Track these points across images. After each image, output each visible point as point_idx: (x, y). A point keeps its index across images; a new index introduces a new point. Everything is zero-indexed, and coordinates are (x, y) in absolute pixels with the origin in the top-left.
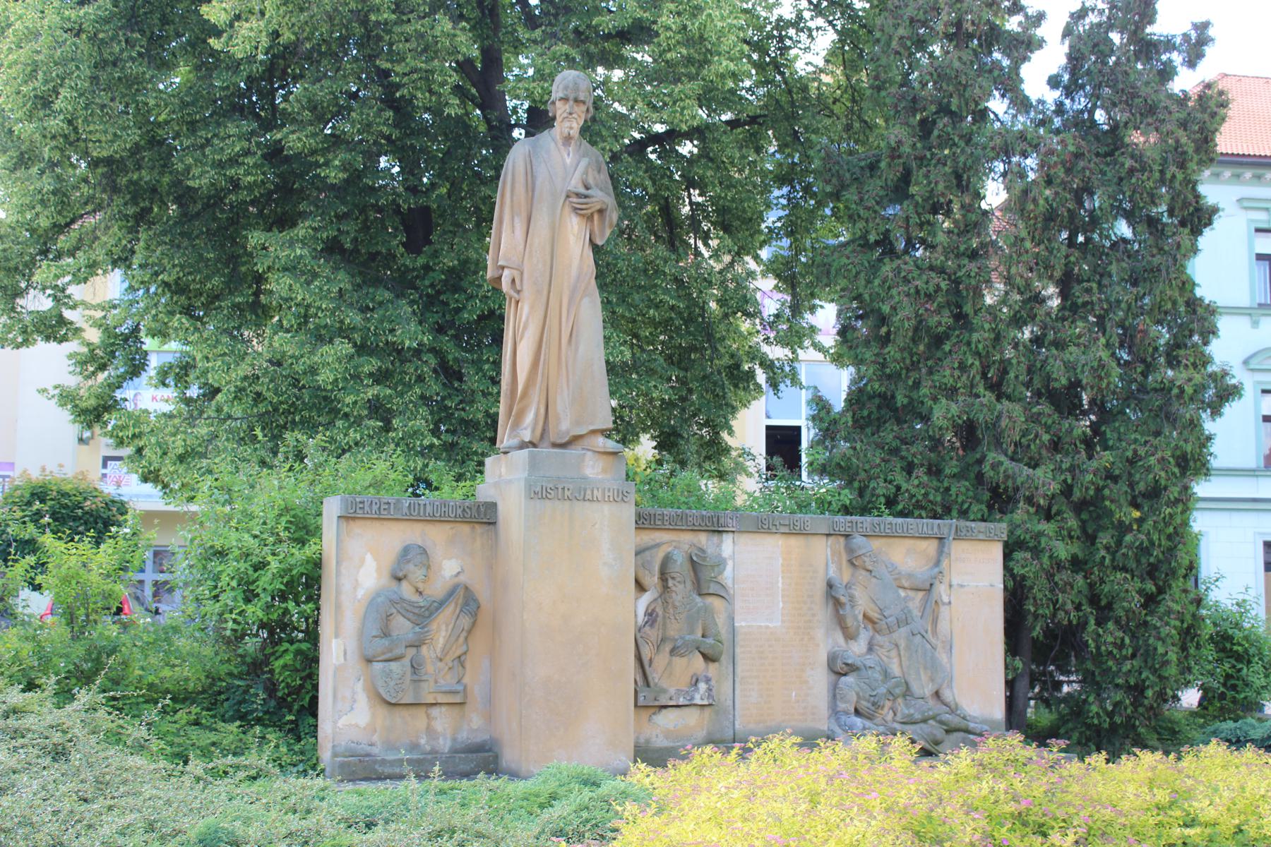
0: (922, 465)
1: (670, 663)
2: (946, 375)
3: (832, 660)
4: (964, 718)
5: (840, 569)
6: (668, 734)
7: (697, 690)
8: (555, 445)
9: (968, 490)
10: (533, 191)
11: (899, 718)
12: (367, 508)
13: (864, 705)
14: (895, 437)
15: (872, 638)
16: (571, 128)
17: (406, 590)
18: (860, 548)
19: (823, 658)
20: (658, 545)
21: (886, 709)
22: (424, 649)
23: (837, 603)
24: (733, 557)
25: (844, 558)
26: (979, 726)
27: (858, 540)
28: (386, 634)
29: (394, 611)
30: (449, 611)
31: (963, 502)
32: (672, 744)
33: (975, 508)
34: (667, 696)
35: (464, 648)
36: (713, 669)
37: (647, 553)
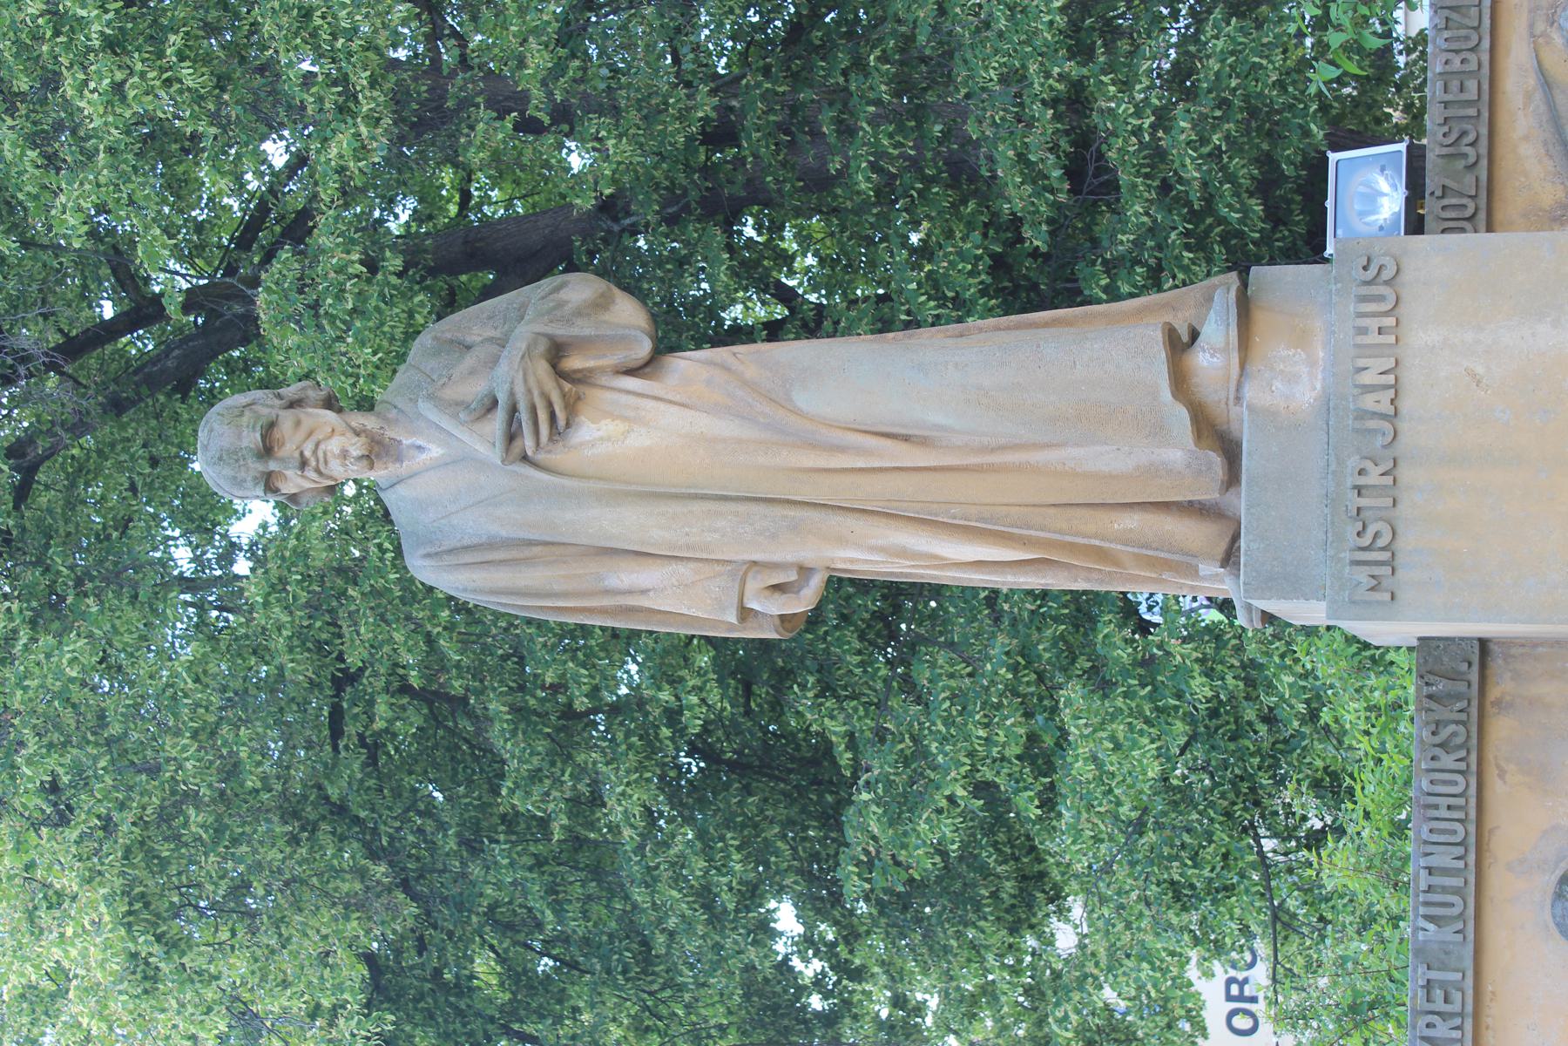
10: (530, 543)
16: (344, 454)
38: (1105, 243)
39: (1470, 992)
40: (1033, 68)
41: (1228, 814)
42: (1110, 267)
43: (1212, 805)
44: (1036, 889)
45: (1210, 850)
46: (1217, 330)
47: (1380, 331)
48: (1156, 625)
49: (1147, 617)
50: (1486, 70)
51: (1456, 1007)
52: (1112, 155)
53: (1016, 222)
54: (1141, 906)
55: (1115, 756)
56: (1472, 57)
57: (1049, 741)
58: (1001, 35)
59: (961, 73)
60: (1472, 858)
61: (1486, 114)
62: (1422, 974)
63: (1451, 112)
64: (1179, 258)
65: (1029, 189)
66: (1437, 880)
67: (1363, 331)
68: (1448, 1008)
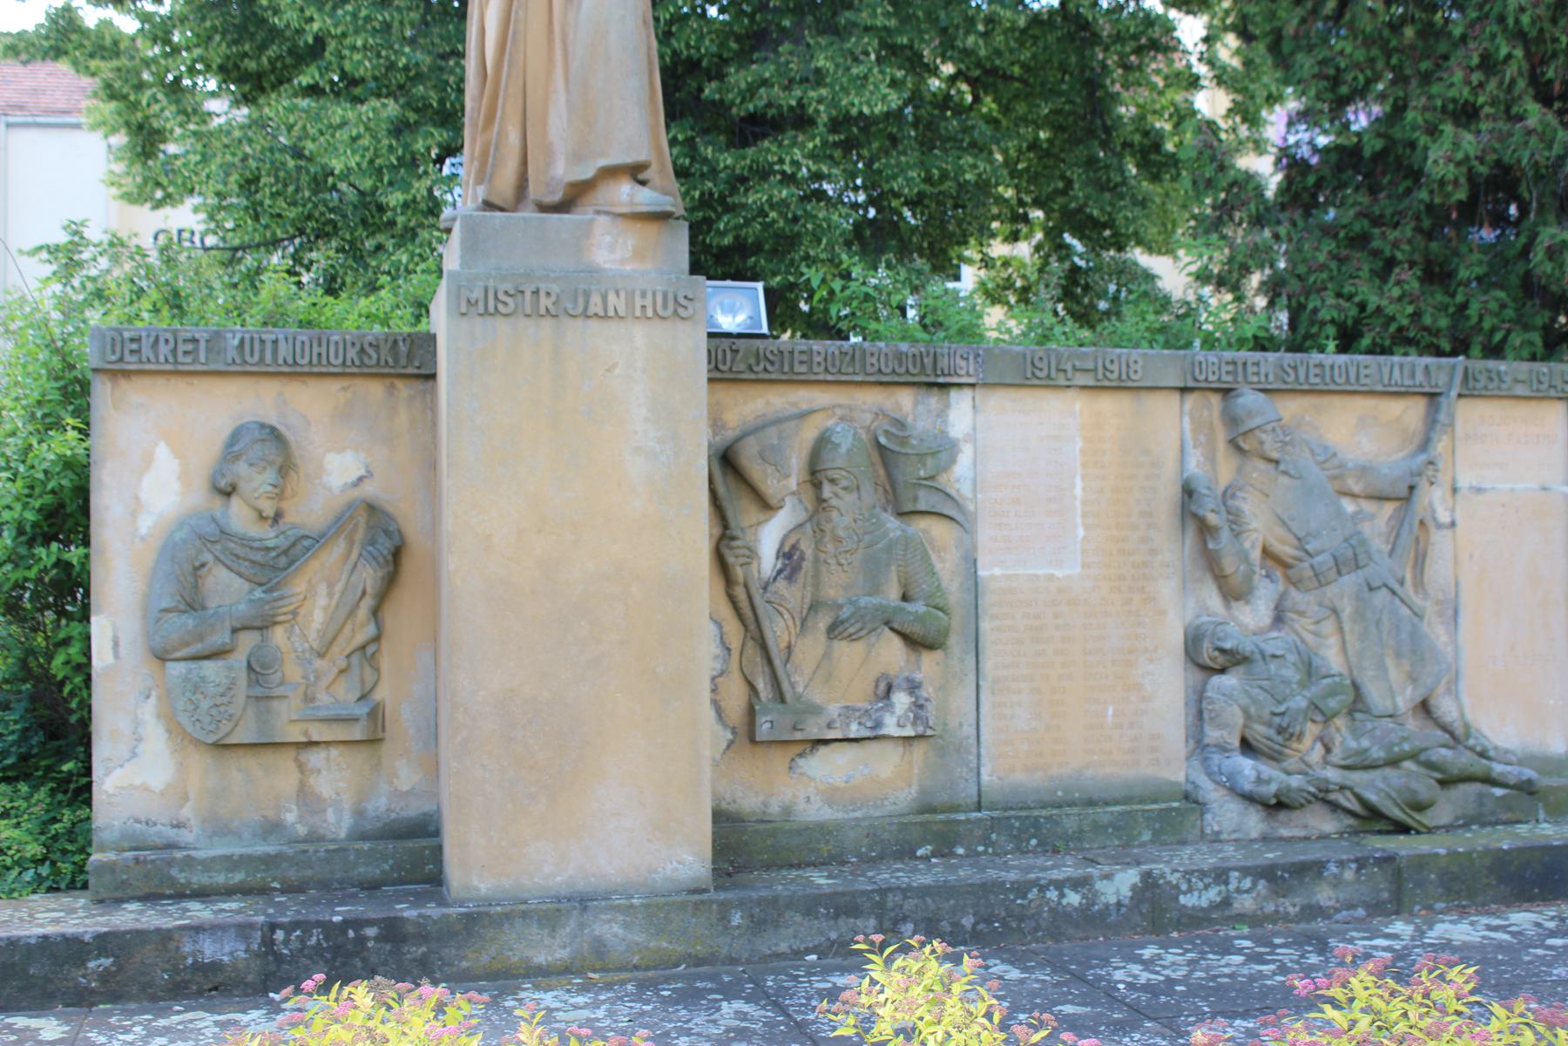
0: (1412, 264)
1: (827, 655)
2: (1456, 83)
3: (1193, 642)
4: (1483, 754)
5: (1212, 459)
6: (831, 796)
7: (889, 707)
8: (544, 208)
9: (1503, 306)
11: (1337, 756)
12: (147, 352)
13: (1259, 732)
14: (1360, 215)
15: (1283, 597)
17: (239, 516)
18: (1250, 414)
19: (1176, 638)
20: (803, 416)
21: (1307, 741)
22: (278, 635)
23: (1205, 530)
24: (972, 438)
25: (1221, 436)
26: (1514, 770)
27: (1249, 399)
28: (192, 603)
29: (208, 557)
30: (332, 556)
31: (1493, 330)
32: (840, 815)
33: (1516, 339)
34: (823, 721)
35: (371, 630)
36: (929, 666)
37: (772, 432)
38: (707, 138)
39: (192, 368)
40: (824, 92)
41: (309, 217)
42: (690, 142)
43: (316, 206)
44: (251, 84)
45: (284, 205)
46: (646, 198)
47: (644, 307)
48: (441, 170)
49: (448, 161)
50: (813, 377)
51: (181, 358)
52: (766, 144)
53: (721, 77)
54: (240, 155)
55: (348, 136)
56: (822, 369)
57: (358, 91)
58: (848, 69)
59: (823, 41)
60: (286, 369)
61: (784, 377)
62: (203, 336)
63: (786, 355)
64: (695, 188)
65: (743, 85)
66: (269, 346)
67: (644, 295)
68: (180, 353)
